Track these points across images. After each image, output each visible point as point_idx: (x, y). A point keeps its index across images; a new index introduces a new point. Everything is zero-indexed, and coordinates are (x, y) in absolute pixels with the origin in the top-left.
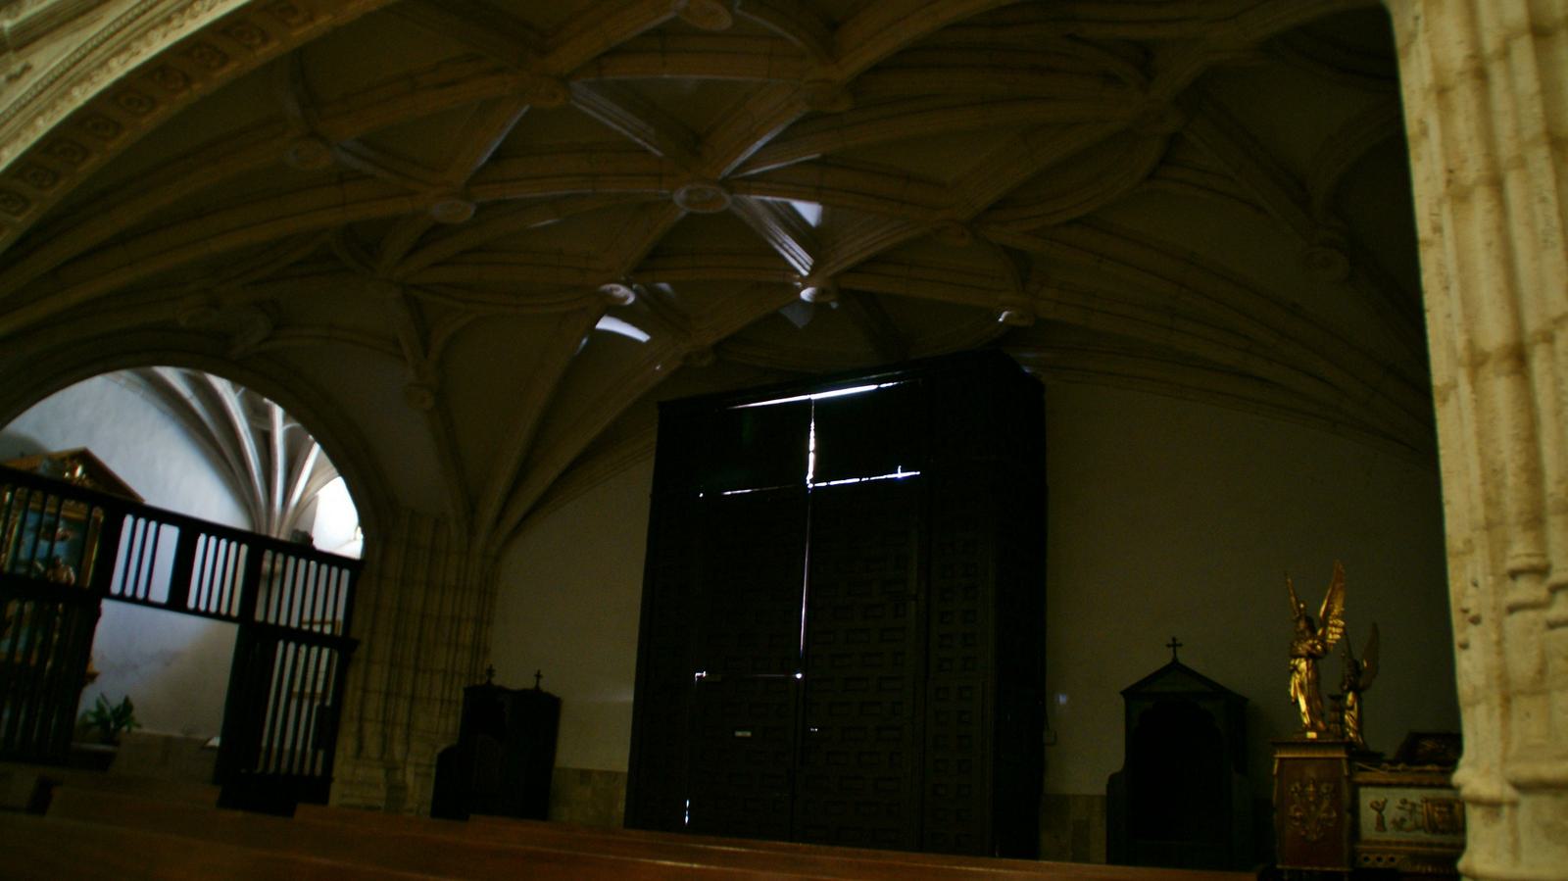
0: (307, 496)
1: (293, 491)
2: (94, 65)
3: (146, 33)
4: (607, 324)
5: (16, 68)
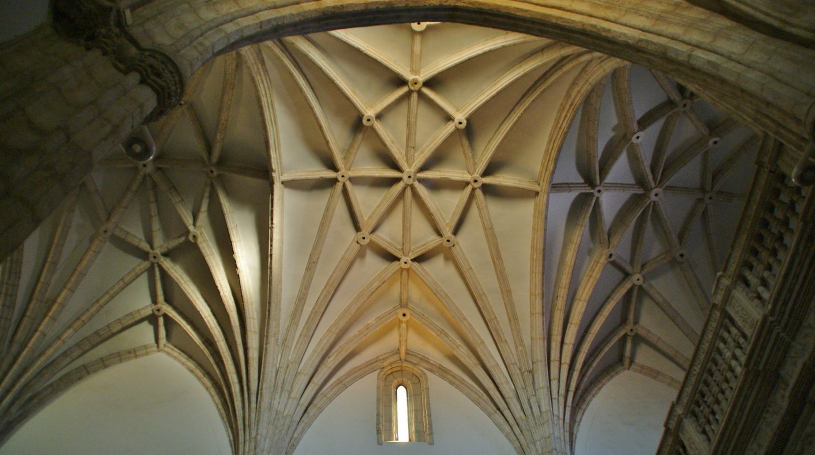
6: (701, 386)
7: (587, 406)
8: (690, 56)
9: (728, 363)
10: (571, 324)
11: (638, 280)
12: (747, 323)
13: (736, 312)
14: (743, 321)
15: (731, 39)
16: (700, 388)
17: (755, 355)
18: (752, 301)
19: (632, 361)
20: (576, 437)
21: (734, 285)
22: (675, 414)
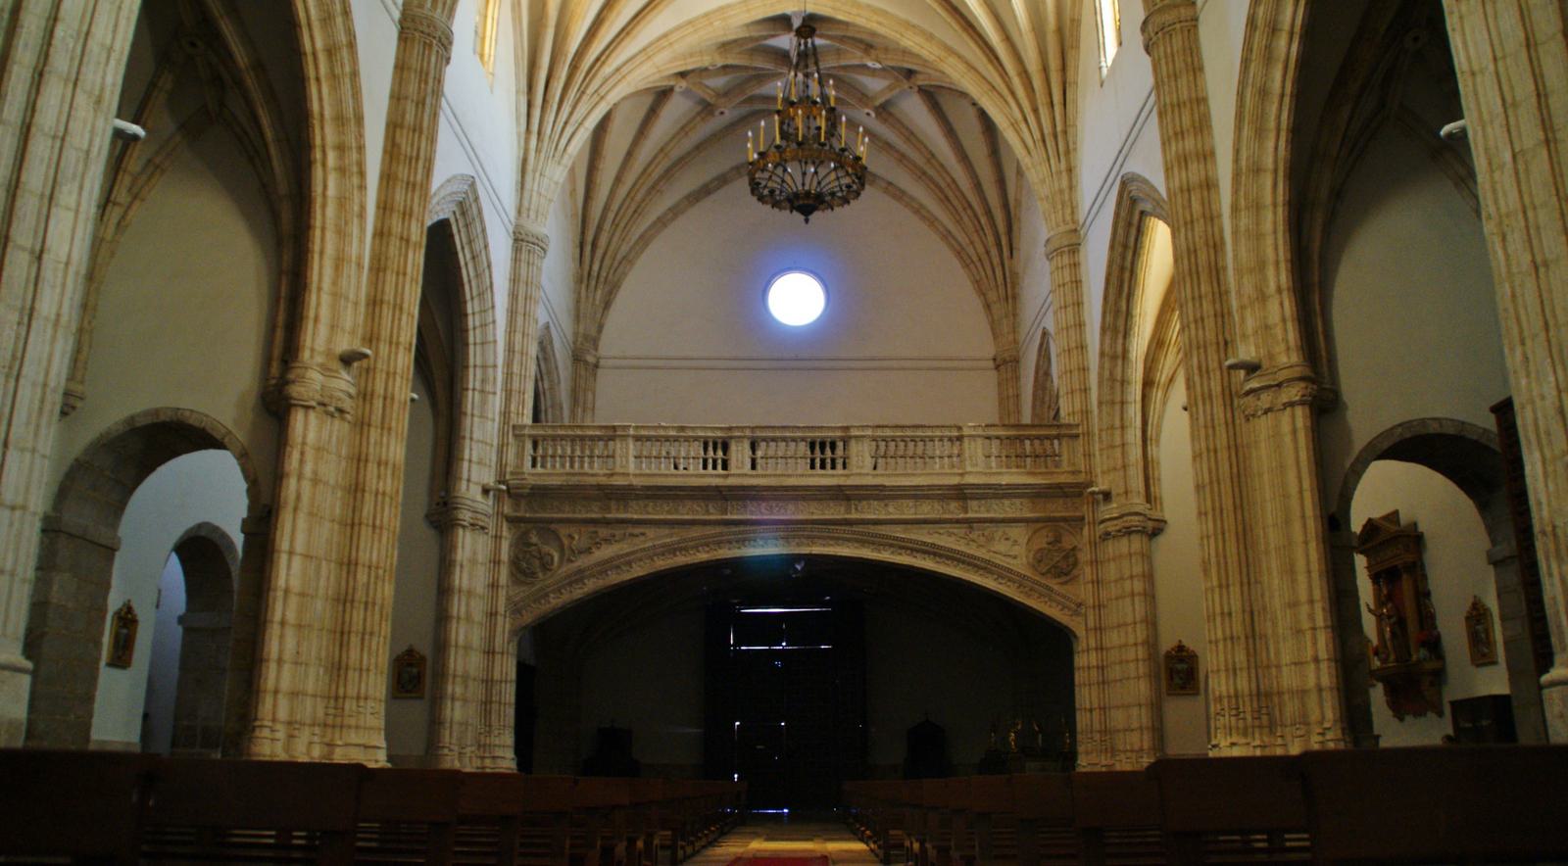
11: (722, 113)
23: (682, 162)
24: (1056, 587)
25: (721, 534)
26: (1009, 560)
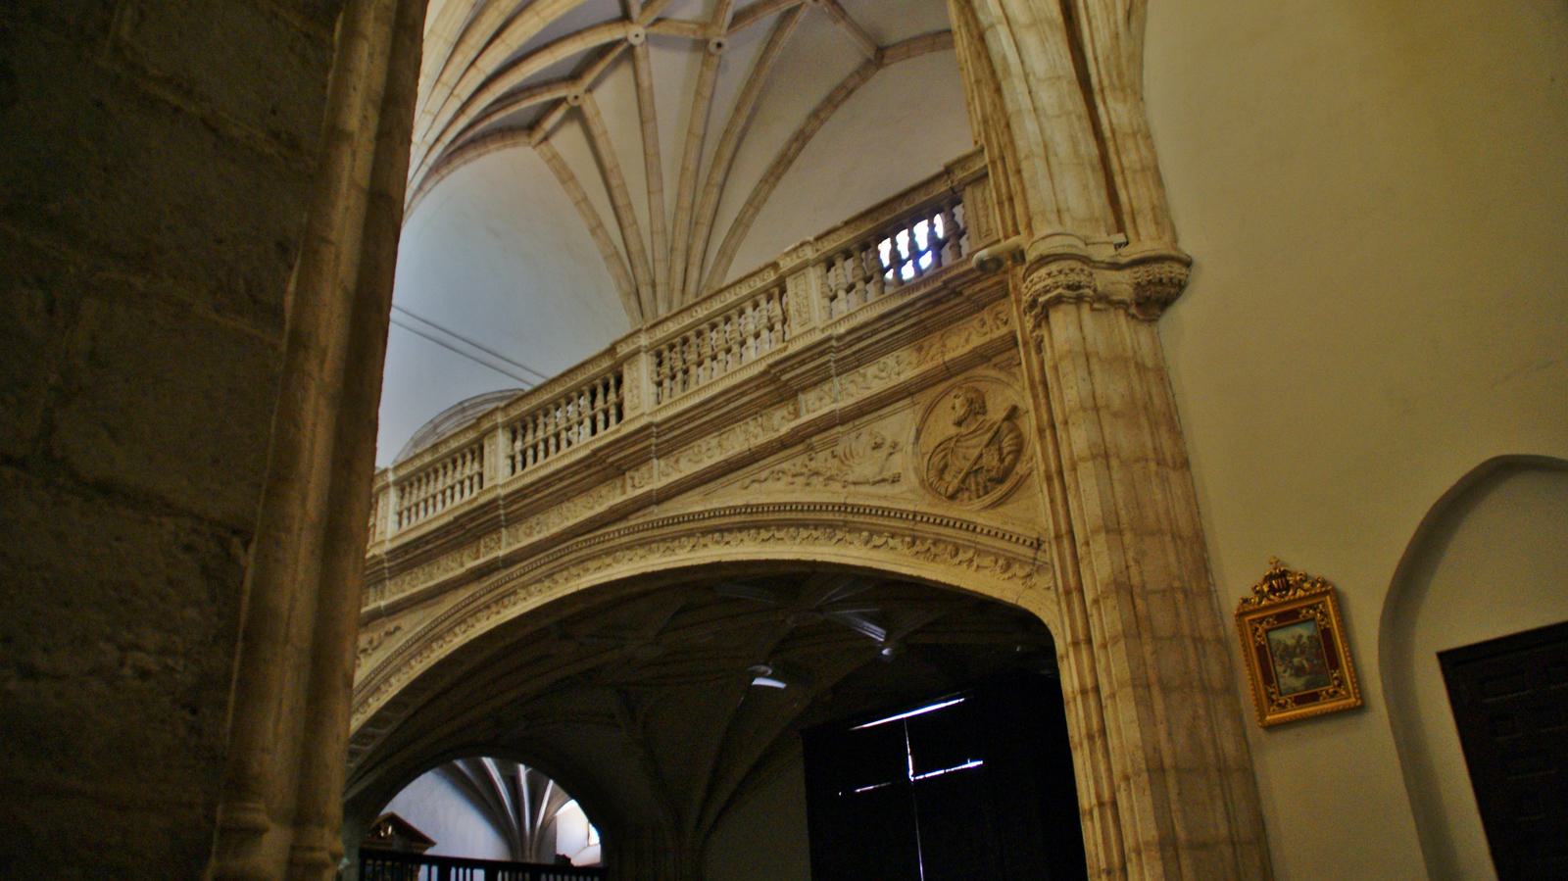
0: (549, 816)
1: (536, 822)
2: (445, 630)
3: (475, 614)
4: (758, 682)
5: (391, 626)
6: (691, 334)
7: (449, 173)
8: (992, 26)
9: (744, 336)
10: (503, 41)
11: (637, 36)
12: (800, 315)
13: (796, 294)
14: (797, 310)
15: (1044, 46)
16: (688, 334)
17: (789, 363)
18: (823, 297)
19: (546, 139)
20: (412, 213)
21: (816, 263)
22: (635, 340)
23: (737, 137)
24: (983, 519)
25: (474, 598)
26: (885, 489)
